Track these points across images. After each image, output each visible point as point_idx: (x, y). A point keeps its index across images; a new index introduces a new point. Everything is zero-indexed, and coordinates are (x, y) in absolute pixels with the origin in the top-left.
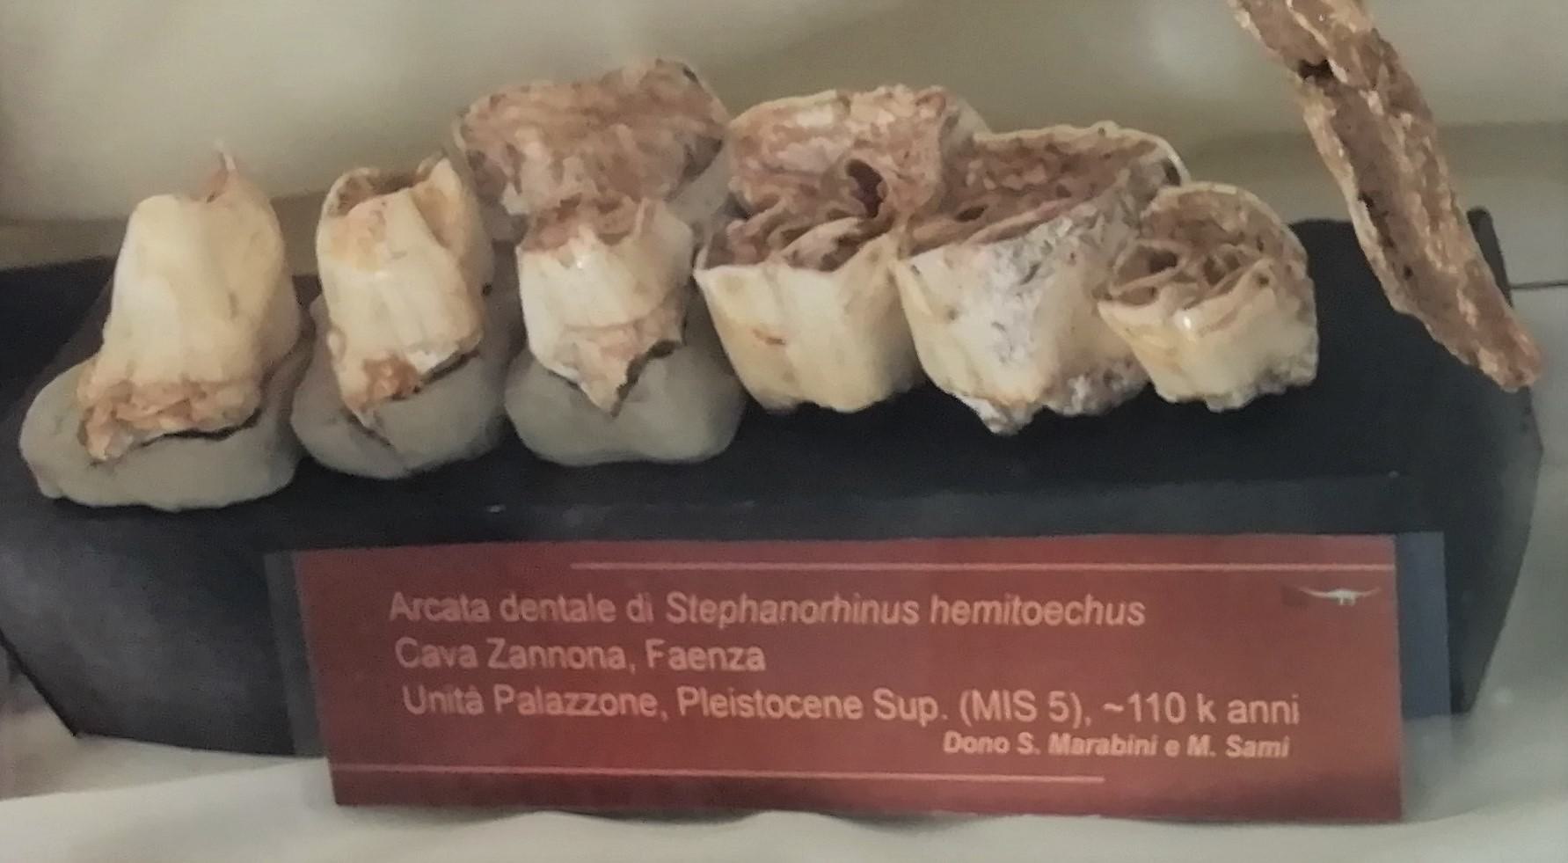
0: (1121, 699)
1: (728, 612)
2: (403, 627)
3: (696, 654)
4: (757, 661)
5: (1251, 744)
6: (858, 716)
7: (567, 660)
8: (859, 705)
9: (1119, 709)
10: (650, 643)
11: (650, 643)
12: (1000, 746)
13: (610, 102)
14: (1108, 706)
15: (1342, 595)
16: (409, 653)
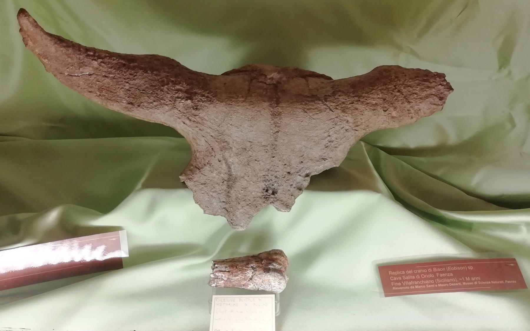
0: (462, 278)
1: (396, 273)
2: (391, 275)
3: (443, 274)
4: (452, 275)
5: (429, 286)
6: (472, 278)
7: (428, 276)
8: (400, 284)
9: (461, 279)
10: (437, 274)
11: (437, 274)
12: (424, 287)
13: (130, 102)
14: (460, 279)
15: (512, 265)
16: (392, 278)
